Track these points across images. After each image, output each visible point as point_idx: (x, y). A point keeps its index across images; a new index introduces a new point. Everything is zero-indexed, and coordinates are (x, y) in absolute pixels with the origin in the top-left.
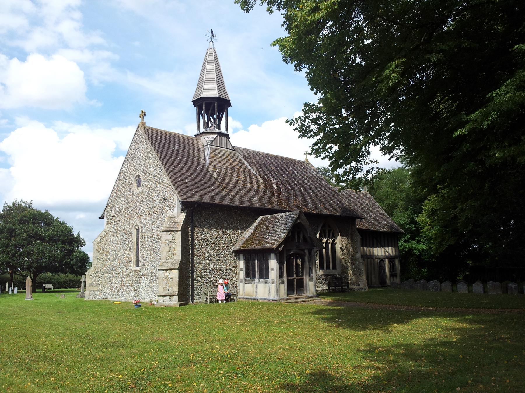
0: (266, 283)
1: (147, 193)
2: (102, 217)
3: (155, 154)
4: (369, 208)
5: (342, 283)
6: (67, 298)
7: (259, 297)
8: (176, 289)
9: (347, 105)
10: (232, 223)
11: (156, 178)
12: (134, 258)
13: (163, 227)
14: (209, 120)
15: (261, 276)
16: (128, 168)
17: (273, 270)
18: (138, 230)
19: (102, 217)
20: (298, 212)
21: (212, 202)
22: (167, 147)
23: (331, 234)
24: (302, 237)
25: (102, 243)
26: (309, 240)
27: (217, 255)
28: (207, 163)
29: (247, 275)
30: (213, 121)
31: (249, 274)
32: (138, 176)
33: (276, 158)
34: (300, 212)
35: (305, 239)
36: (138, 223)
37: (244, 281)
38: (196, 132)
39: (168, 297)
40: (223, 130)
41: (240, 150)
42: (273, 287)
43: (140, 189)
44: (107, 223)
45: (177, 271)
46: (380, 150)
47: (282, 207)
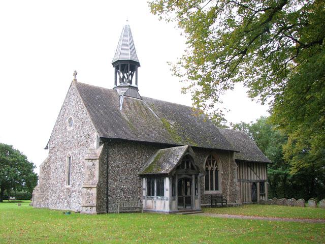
0: (162, 199)
1: (76, 131)
2: (46, 148)
3: (82, 102)
4: (245, 144)
5: (222, 200)
6: (25, 205)
7: (157, 210)
8: (95, 202)
9: (223, 53)
10: (137, 154)
11: (83, 120)
12: (66, 179)
13: (86, 156)
14: (124, 77)
15: (158, 194)
16: (64, 112)
17: (167, 190)
18: (70, 158)
19: (46, 148)
20: (187, 146)
21: (123, 138)
22: (92, 98)
23: (215, 163)
24: (190, 165)
25: (46, 166)
26: (195, 167)
27: (126, 178)
28: (121, 109)
29: (149, 194)
30: (126, 77)
31: (150, 193)
32: (71, 118)
33: (174, 105)
34: (189, 147)
35: (192, 168)
36: (70, 152)
37: (146, 198)
38: (114, 86)
39: (89, 208)
40: (134, 84)
41: (146, 99)
42: (167, 203)
43: (72, 128)
44: (50, 153)
45: (95, 189)
46: (252, 96)
47: (180, 143)
